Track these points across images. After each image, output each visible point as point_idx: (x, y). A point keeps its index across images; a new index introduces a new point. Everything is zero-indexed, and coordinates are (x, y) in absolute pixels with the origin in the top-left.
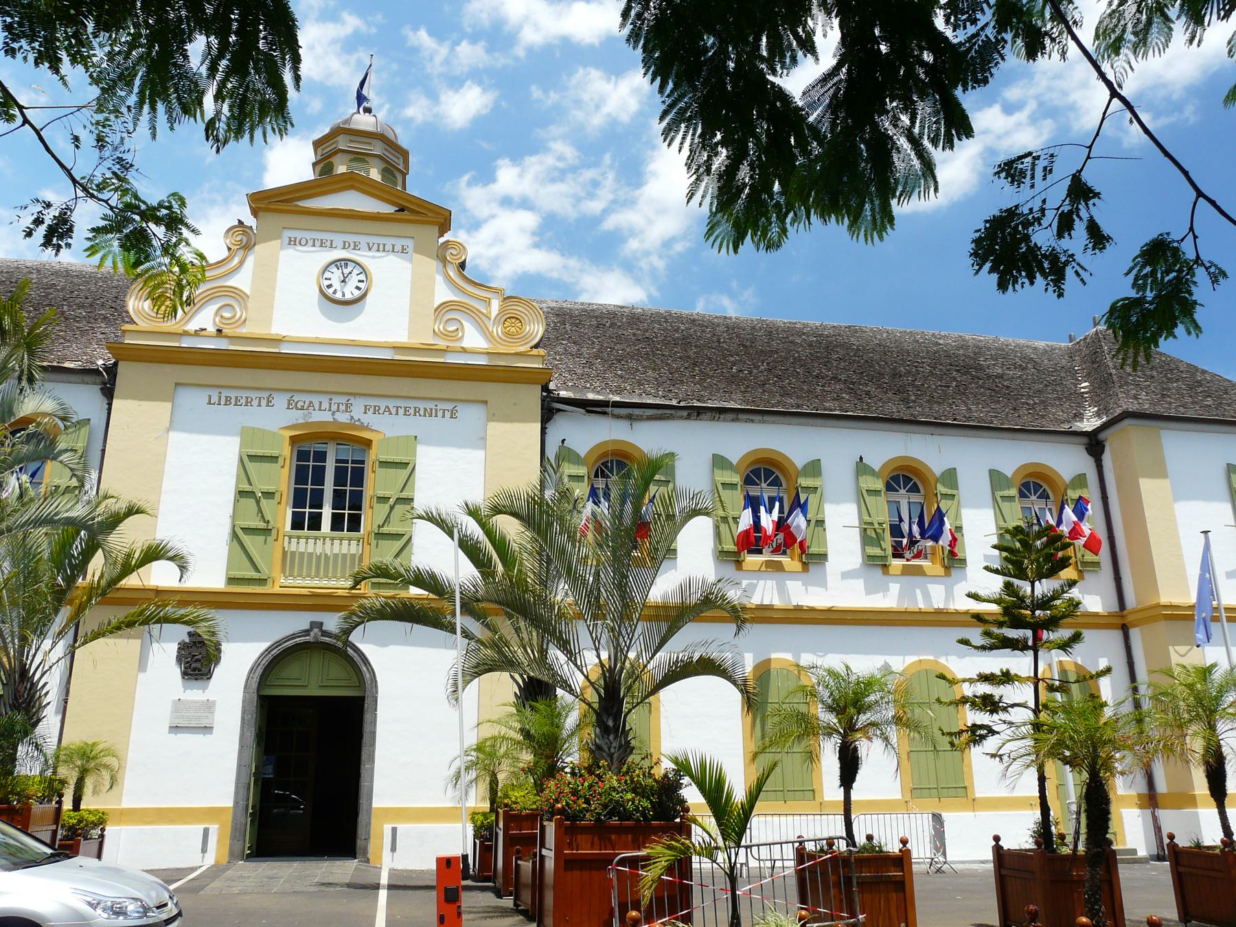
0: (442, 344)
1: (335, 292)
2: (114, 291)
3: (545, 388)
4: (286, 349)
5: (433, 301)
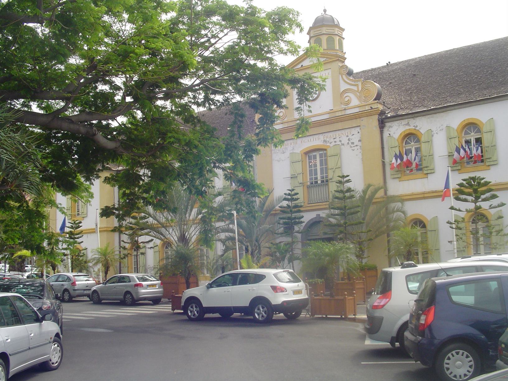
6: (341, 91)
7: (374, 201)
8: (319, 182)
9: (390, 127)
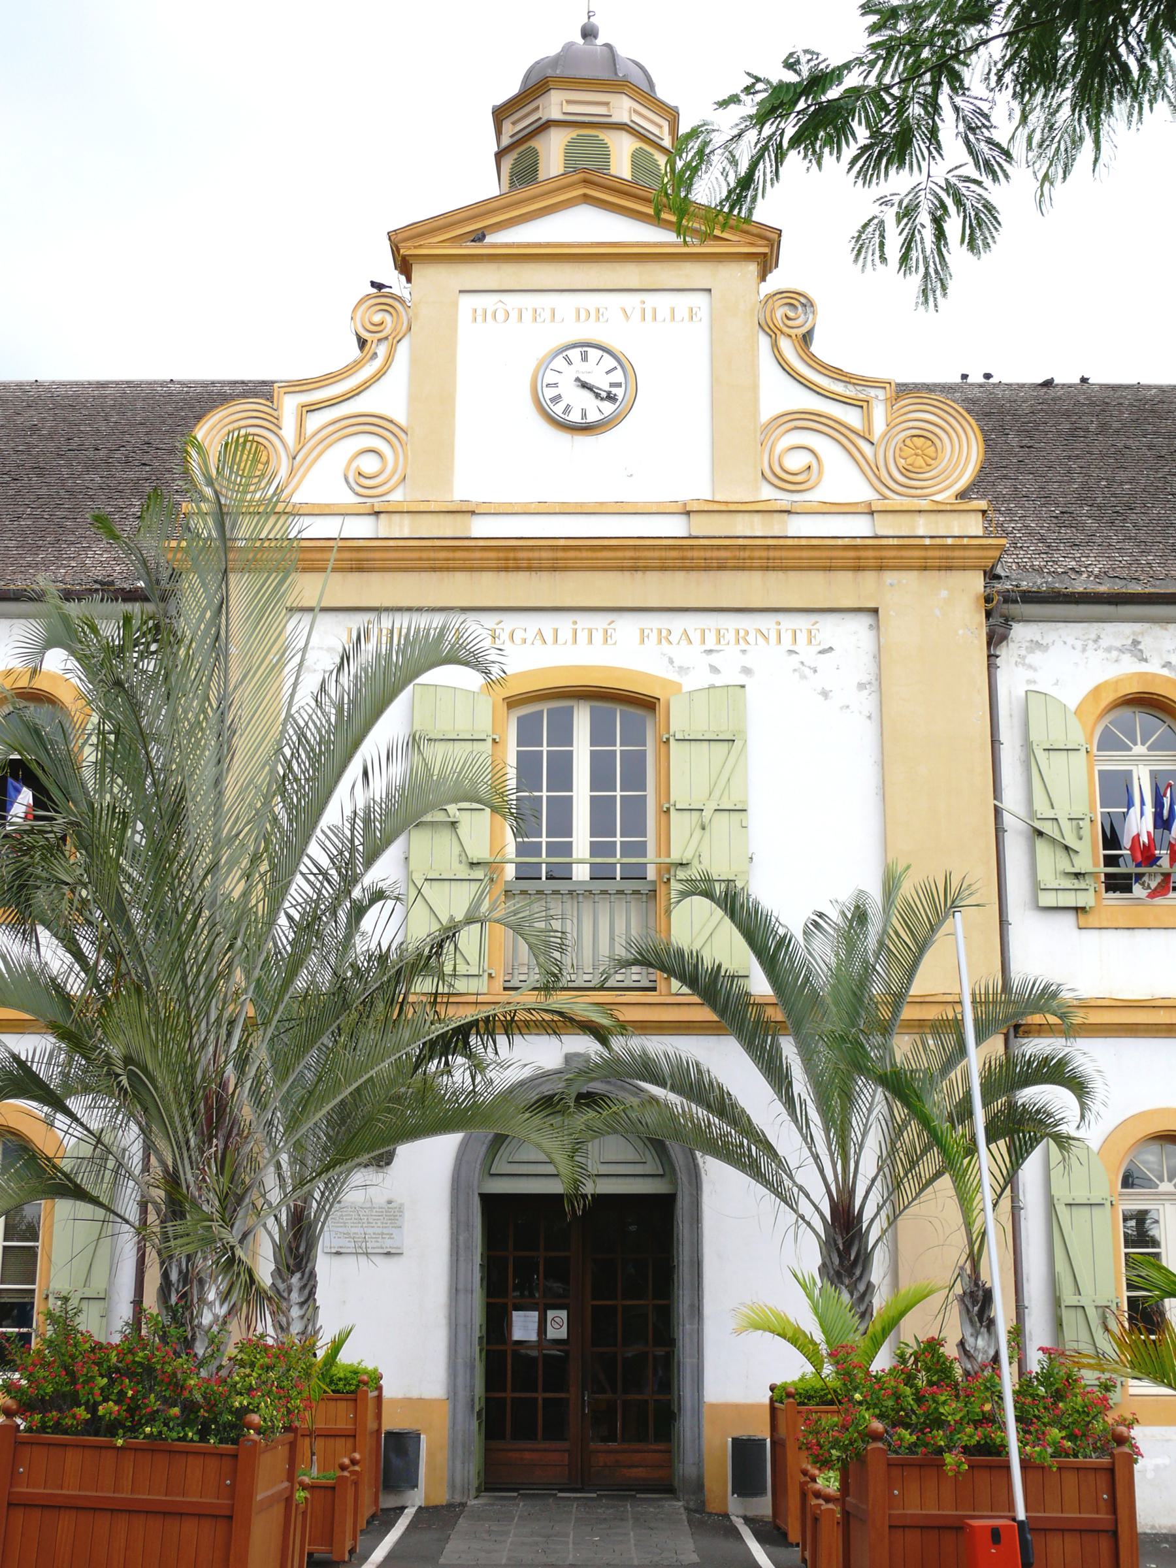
0: (785, 499)
1: (567, 409)
2: (142, 429)
3: (991, 576)
4: (482, 528)
5: (756, 412)
6: (765, 415)
7: (908, 1013)
8: (581, 873)
9: (1036, 646)
